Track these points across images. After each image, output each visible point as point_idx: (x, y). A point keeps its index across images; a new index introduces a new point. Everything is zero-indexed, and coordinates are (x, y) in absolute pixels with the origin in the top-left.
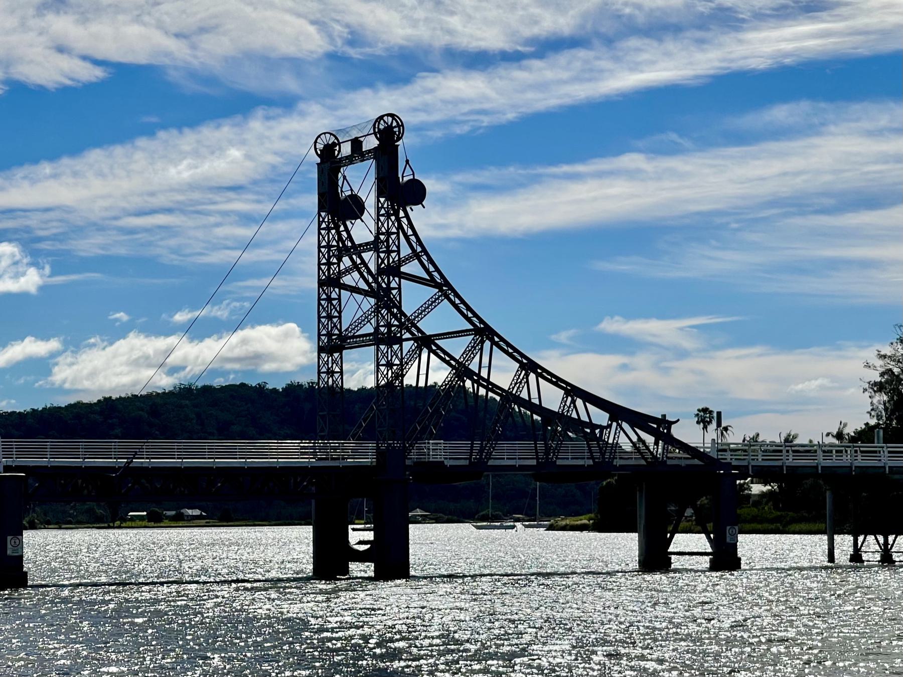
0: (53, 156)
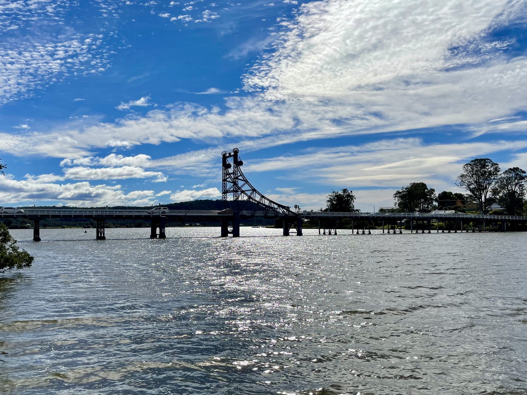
0: (170, 156)
